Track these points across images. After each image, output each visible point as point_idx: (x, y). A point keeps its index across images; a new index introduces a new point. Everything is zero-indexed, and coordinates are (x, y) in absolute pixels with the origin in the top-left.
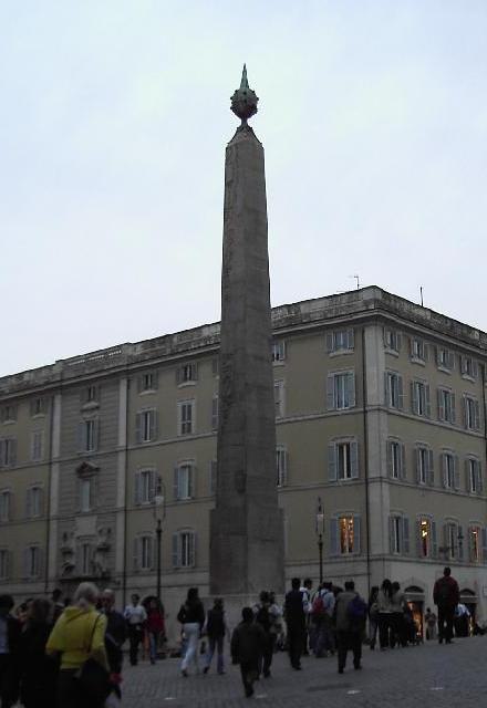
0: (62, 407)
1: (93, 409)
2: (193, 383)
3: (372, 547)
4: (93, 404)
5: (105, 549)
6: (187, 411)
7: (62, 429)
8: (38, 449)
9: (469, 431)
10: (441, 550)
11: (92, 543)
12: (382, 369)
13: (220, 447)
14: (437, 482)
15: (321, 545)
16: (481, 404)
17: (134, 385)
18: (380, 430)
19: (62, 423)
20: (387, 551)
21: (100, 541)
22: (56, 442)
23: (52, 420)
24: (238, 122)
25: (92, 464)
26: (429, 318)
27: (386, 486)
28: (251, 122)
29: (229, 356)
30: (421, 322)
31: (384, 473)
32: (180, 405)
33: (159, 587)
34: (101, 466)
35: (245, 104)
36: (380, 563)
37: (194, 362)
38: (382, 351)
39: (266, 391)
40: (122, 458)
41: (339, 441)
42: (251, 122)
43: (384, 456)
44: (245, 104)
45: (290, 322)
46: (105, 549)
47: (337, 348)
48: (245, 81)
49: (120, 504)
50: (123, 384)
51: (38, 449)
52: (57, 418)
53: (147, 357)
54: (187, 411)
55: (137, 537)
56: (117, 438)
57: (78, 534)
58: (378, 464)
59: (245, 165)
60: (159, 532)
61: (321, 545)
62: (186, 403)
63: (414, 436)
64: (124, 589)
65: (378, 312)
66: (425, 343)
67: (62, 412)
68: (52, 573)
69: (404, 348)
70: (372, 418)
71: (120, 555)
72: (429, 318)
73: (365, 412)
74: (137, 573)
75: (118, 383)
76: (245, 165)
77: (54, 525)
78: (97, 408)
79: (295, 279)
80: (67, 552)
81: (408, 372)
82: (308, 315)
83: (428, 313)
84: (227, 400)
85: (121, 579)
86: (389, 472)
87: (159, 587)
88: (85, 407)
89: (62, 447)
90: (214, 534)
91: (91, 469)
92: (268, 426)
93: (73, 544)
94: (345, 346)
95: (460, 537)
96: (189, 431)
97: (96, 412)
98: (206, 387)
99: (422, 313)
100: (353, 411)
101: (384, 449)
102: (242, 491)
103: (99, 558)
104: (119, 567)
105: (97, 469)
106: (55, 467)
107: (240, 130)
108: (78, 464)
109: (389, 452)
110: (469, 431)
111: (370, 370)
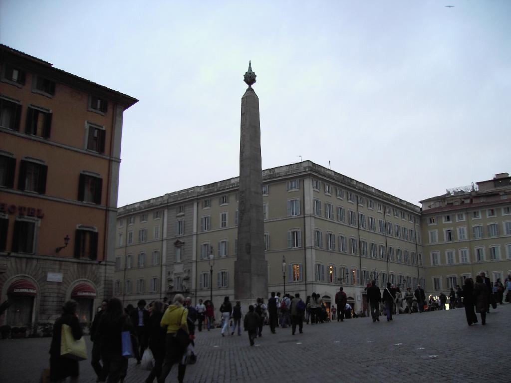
0: (168, 215)
3: (308, 278)
5: (187, 279)
7: (168, 225)
21: (185, 275)
23: (163, 221)
24: (247, 86)
25: (181, 241)
26: (333, 175)
42: (253, 86)
46: (187, 279)
47: (291, 188)
49: (194, 259)
52: (165, 220)
55: (202, 273)
58: (310, 241)
64: (196, 297)
68: (163, 290)
72: (333, 175)
73: (304, 217)
75: (193, 204)
77: (164, 268)
78: (184, 215)
82: (278, 173)
83: (374, 189)
88: (178, 215)
94: (295, 187)
97: (183, 217)
99: (330, 172)
104: (193, 287)
105: (184, 243)
108: (175, 241)
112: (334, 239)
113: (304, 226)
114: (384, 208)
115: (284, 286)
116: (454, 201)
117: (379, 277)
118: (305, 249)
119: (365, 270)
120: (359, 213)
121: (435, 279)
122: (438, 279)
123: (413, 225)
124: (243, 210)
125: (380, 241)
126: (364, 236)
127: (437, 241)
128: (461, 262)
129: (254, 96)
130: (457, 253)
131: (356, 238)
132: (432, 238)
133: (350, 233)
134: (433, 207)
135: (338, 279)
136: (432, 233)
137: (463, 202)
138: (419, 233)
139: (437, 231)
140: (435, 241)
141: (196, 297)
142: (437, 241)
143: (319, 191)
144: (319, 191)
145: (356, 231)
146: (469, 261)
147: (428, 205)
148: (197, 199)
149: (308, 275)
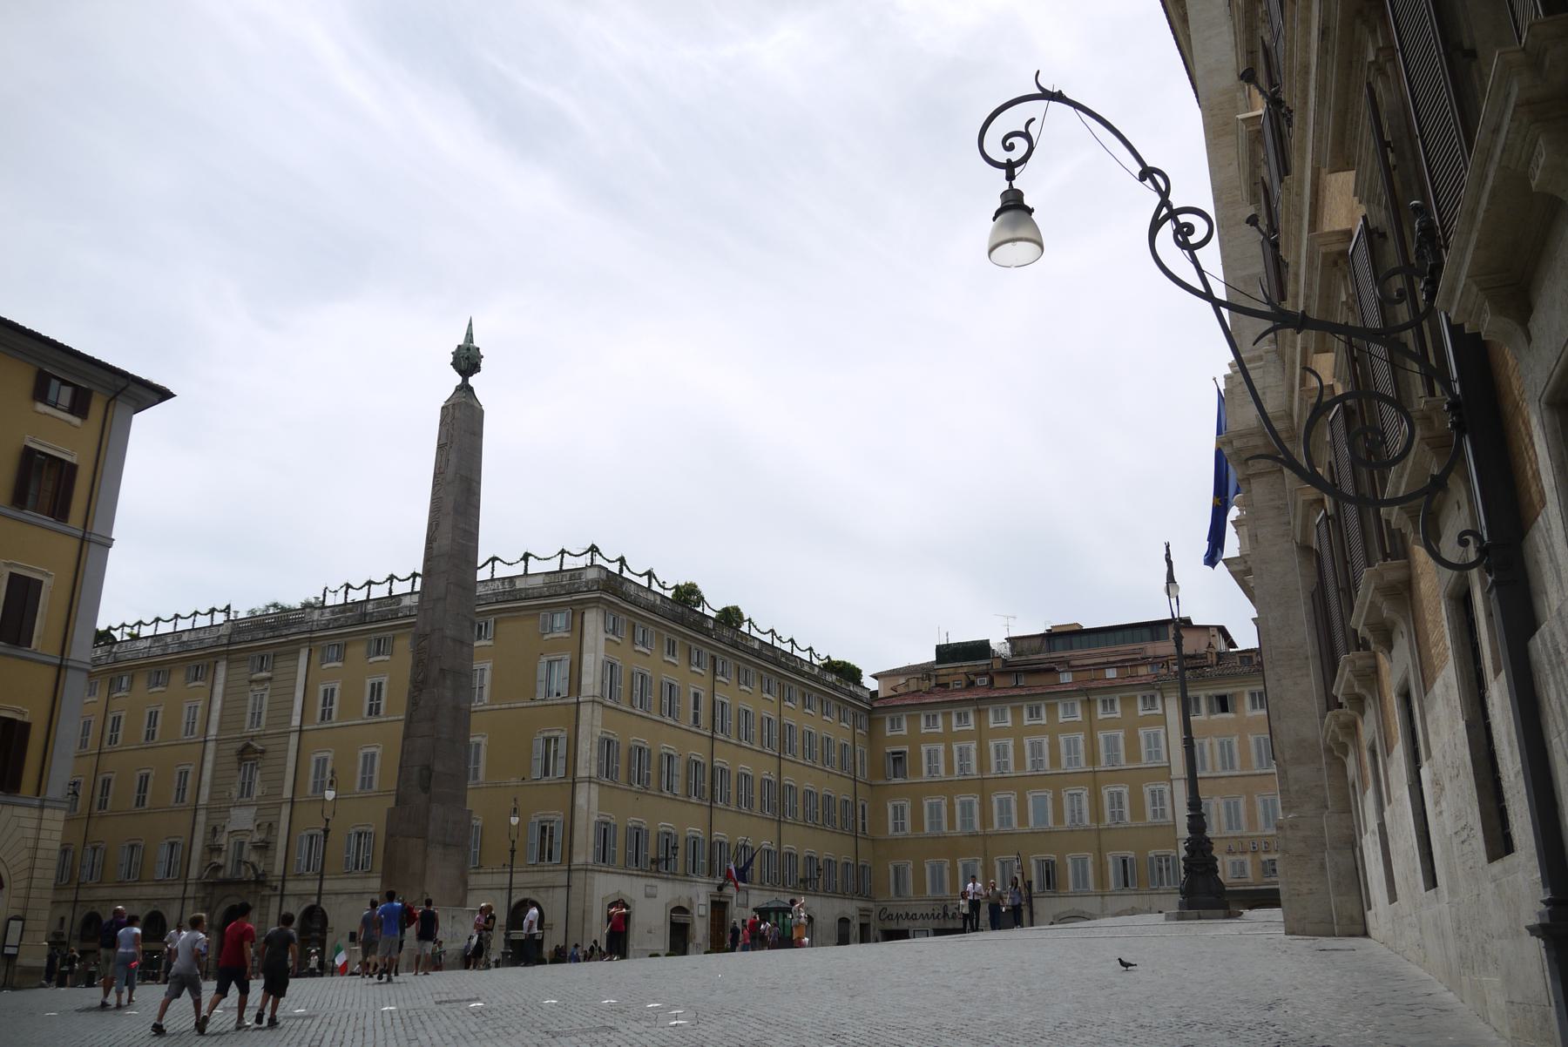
1: (263, 681)
4: (264, 674)
6: (376, 690)
9: (744, 743)
10: (653, 861)
12: (602, 656)
13: (407, 736)
14: (654, 783)
15: (513, 851)
17: (316, 657)
18: (592, 725)
20: (590, 860)
21: (257, 837)
22: (265, 708)
24: (458, 379)
27: (595, 789)
28: (472, 381)
29: (425, 636)
31: (594, 773)
32: (322, 688)
33: (319, 895)
35: (467, 361)
36: (582, 874)
37: (390, 634)
38: (602, 636)
39: (463, 678)
40: (294, 739)
42: (472, 381)
43: (595, 754)
44: (467, 361)
45: (500, 597)
46: (264, 847)
48: (469, 336)
54: (376, 690)
56: (290, 716)
57: (230, 828)
59: (461, 427)
60: (326, 831)
61: (513, 851)
62: (376, 680)
63: (634, 734)
65: (601, 591)
66: (651, 628)
67: (227, 681)
68: (194, 873)
69: (626, 635)
70: (585, 711)
71: (280, 855)
74: (299, 877)
75: (297, 652)
76: (461, 427)
78: (270, 679)
79: (520, 531)
80: (214, 849)
84: (419, 685)
85: (279, 884)
86: (600, 771)
87: (319, 895)
89: (221, 722)
90: (390, 835)
91: (256, 751)
92: (461, 718)
93: (223, 839)
95: (819, 869)
96: (377, 713)
98: (392, 671)
101: (595, 746)
102: (426, 789)
103: (253, 858)
104: (278, 869)
105: (263, 752)
107: (458, 389)
108: (240, 745)
109: (600, 749)
110: (744, 743)
111: (588, 659)
114: (855, 716)
118: (574, 783)
125: (763, 769)
134: (901, 690)
138: (862, 753)
148: (310, 640)
149: (575, 850)
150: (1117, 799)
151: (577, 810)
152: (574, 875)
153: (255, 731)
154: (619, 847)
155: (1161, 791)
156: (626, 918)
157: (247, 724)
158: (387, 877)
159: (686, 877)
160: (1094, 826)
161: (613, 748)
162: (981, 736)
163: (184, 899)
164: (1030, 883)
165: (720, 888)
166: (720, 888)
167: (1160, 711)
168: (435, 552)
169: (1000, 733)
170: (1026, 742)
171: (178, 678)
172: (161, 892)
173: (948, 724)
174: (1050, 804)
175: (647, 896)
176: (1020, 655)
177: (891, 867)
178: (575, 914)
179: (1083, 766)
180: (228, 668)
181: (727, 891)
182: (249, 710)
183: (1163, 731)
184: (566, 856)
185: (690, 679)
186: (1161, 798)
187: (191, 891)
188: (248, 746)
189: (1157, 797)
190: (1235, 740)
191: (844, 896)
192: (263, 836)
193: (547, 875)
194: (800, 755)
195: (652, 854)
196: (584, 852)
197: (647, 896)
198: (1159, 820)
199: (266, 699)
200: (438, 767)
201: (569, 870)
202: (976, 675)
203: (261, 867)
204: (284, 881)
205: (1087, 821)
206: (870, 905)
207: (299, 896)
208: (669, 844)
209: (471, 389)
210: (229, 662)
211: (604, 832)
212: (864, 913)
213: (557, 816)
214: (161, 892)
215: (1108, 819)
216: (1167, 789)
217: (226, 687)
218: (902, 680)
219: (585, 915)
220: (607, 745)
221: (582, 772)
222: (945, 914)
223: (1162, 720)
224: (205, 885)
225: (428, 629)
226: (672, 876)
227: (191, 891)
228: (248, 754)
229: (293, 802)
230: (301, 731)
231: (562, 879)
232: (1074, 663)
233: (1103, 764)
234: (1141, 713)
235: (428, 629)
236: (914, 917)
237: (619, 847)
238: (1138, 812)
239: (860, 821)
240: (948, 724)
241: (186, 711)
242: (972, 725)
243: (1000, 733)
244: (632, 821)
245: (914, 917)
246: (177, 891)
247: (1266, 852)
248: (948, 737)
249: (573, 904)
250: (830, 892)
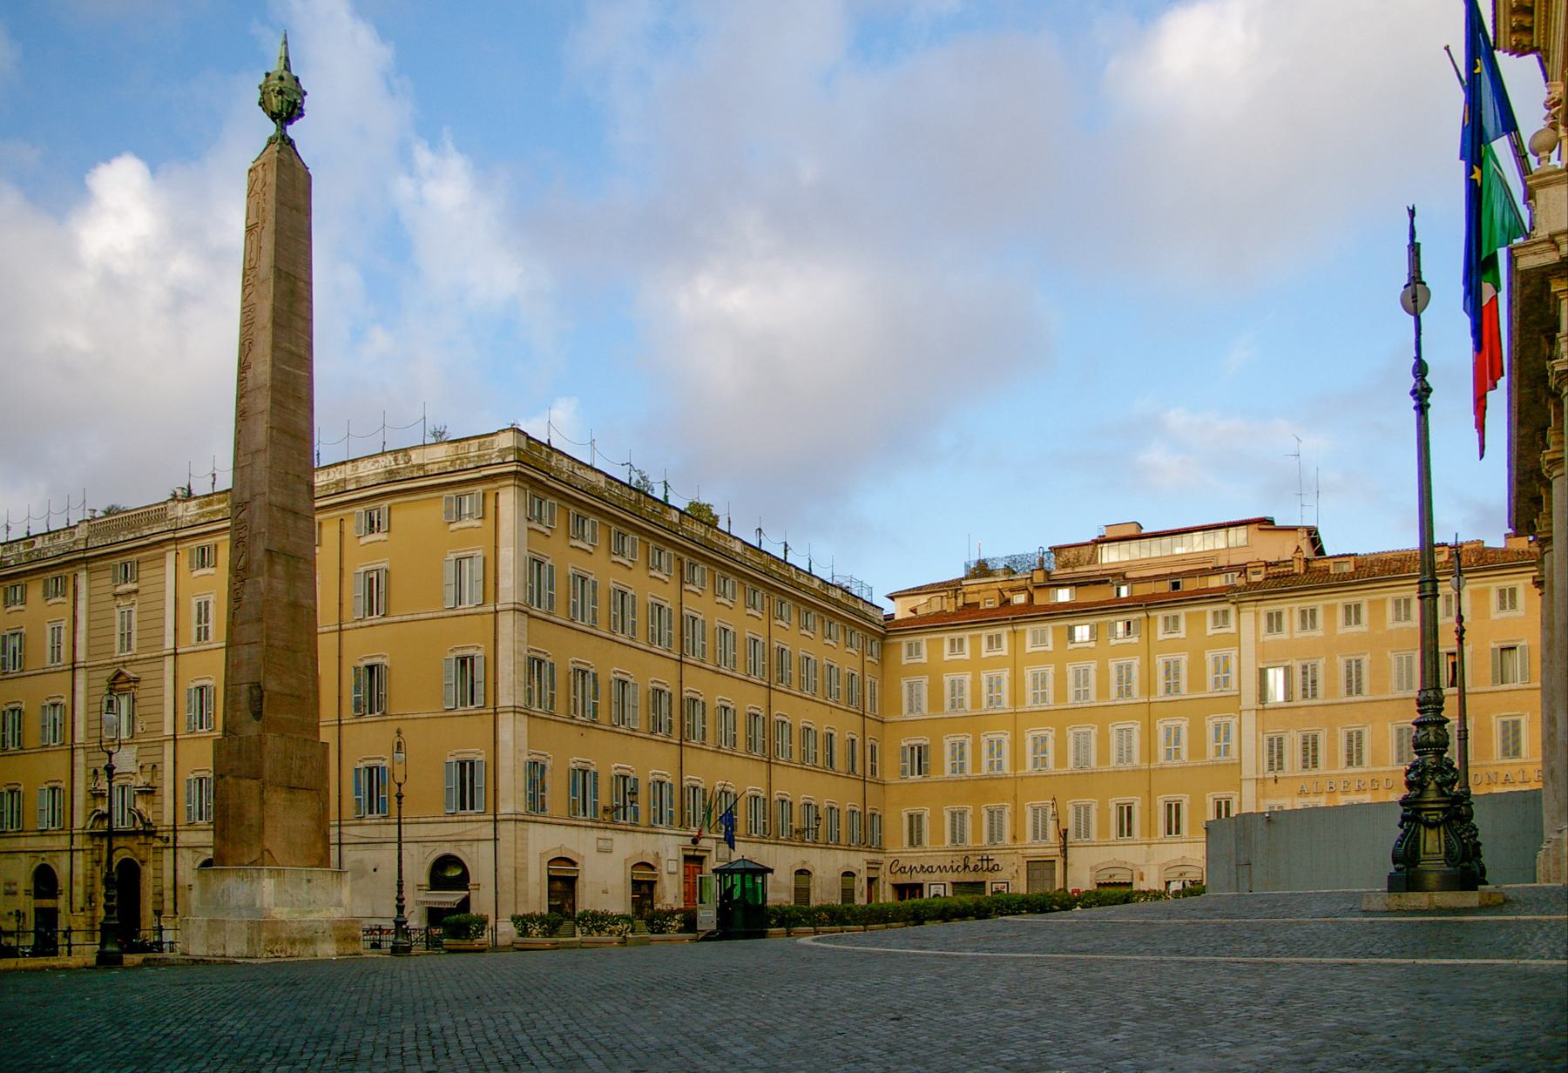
0: (90, 589)
1: (129, 593)
2: (212, 571)
3: (501, 805)
5: (149, 792)
7: (89, 621)
8: (56, 648)
11: (133, 783)
16: (675, 613)
19: (89, 612)
20: (522, 810)
21: (141, 781)
23: (75, 607)
24: (271, 128)
25: (129, 672)
26: (602, 484)
30: (591, 491)
32: (194, 602)
34: (144, 676)
41: (460, 653)
42: (292, 130)
46: (149, 792)
47: (460, 517)
49: (168, 731)
50: (171, 556)
51: (56, 648)
52: (82, 605)
53: (203, 520)
55: (192, 776)
58: (510, 688)
62: (203, 599)
64: (175, 847)
68: (79, 822)
72: (602, 484)
73: (496, 612)
75: (163, 557)
77: (80, 758)
78: (136, 591)
81: (566, 558)
82: (421, 466)
83: (603, 478)
88: (119, 589)
94: (470, 515)
95: (818, 818)
97: (134, 598)
99: (591, 476)
100: (479, 610)
103: (140, 805)
104: (168, 819)
105: (137, 680)
106: (81, 676)
108: (110, 673)
112: (596, 689)
113: (496, 641)
114: (865, 639)
115: (399, 824)
116: (985, 595)
117: (741, 803)
118: (496, 714)
119: (696, 783)
120: (685, 611)
121: (911, 816)
122: (920, 817)
123: (859, 658)
124: (243, 569)
125: (748, 700)
126: (698, 684)
127: (925, 708)
128: (985, 771)
129: (292, 165)
130: (976, 746)
131: (671, 687)
132: (911, 700)
133: (651, 672)
134: (921, 612)
135: (606, 810)
136: (910, 686)
137: (1008, 601)
138: (873, 685)
139: (925, 681)
140: (919, 709)
141: (175, 847)
142: (925, 708)
143: (548, 532)
144: (548, 532)
145: (673, 667)
146: (1007, 769)
147: (912, 606)
148: (176, 540)
149: (501, 795)
150: (1173, 736)
151: (501, 748)
152: (501, 826)
153: (126, 656)
154: (557, 792)
155: (1227, 725)
156: (570, 882)
157: (117, 648)
158: (220, 831)
159: (651, 829)
160: (1145, 766)
161: (629, 691)
162: (1016, 663)
163: (72, 851)
164: (1066, 831)
165: (695, 841)
166: (695, 841)
167: (1232, 629)
168: (250, 385)
169: (1034, 659)
170: (1070, 669)
171: (35, 591)
172: (48, 843)
173: (976, 650)
174: (1093, 741)
175: (599, 851)
176: (1064, 566)
177: (905, 816)
178: (506, 873)
179: (1137, 695)
180: (90, 581)
181: (704, 843)
182: (118, 630)
183: (1235, 653)
184: (491, 805)
185: (648, 582)
186: (1227, 733)
187: (79, 842)
188: (120, 674)
189: (1222, 732)
190: (1321, 664)
191: (849, 848)
192: (148, 780)
193: (469, 826)
194: (795, 685)
195: (605, 800)
196: (512, 799)
197: (599, 851)
198: (1222, 759)
199: (134, 615)
200: (272, 685)
201: (496, 821)
202: (1012, 590)
203: (150, 815)
204: (175, 830)
205: (1136, 761)
206: (879, 857)
207: (193, 848)
208: (627, 788)
209: (291, 142)
210: (90, 571)
211: (536, 773)
212: (873, 866)
213: (480, 755)
214: (48, 843)
215: (1030, 767)
216: (1234, 722)
217: (90, 604)
218: (923, 599)
219: (519, 872)
220: (535, 665)
221: (505, 700)
222: (966, 866)
223: (1235, 640)
224: (93, 836)
225: (247, 496)
226: (634, 828)
227: (79, 842)
228: (119, 683)
229: (175, 739)
230: (176, 654)
231: (488, 830)
232: (1129, 575)
233: (1160, 694)
234: (1210, 632)
235: (247, 496)
236: (929, 870)
237: (557, 792)
238: (1197, 749)
239: (869, 763)
240: (976, 650)
241: (49, 633)
242: (1005, 649)
243: (1034, 659)
244: (615, 767)
245: (929, 870)
246: (63, 842)
247: (1344, 792)
248: (976, 664)
249: (502, 862)
250: (832, 843)
